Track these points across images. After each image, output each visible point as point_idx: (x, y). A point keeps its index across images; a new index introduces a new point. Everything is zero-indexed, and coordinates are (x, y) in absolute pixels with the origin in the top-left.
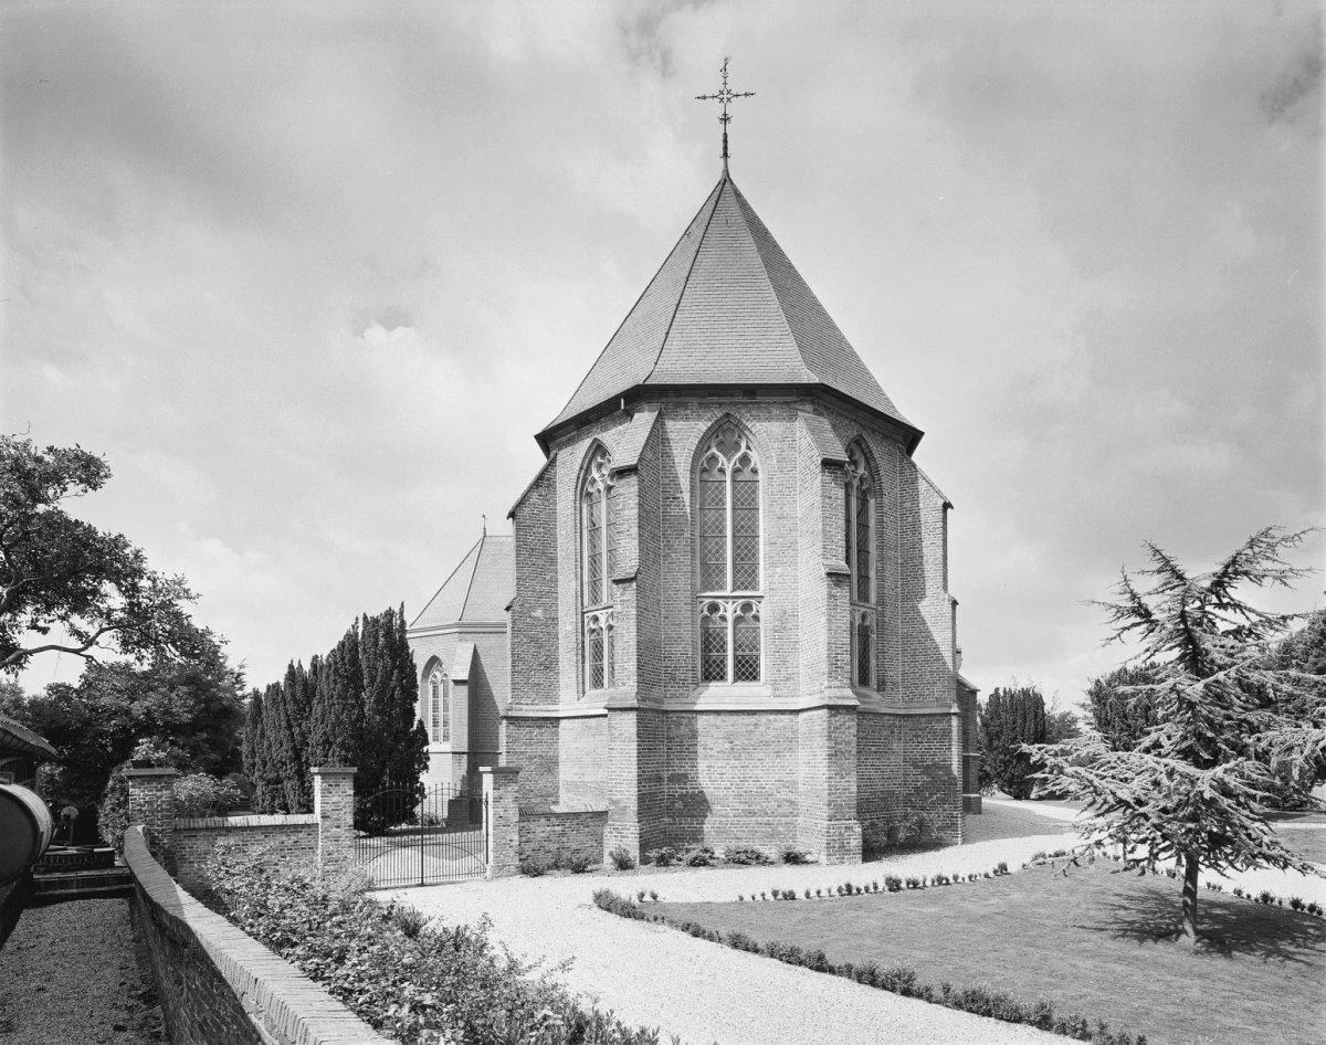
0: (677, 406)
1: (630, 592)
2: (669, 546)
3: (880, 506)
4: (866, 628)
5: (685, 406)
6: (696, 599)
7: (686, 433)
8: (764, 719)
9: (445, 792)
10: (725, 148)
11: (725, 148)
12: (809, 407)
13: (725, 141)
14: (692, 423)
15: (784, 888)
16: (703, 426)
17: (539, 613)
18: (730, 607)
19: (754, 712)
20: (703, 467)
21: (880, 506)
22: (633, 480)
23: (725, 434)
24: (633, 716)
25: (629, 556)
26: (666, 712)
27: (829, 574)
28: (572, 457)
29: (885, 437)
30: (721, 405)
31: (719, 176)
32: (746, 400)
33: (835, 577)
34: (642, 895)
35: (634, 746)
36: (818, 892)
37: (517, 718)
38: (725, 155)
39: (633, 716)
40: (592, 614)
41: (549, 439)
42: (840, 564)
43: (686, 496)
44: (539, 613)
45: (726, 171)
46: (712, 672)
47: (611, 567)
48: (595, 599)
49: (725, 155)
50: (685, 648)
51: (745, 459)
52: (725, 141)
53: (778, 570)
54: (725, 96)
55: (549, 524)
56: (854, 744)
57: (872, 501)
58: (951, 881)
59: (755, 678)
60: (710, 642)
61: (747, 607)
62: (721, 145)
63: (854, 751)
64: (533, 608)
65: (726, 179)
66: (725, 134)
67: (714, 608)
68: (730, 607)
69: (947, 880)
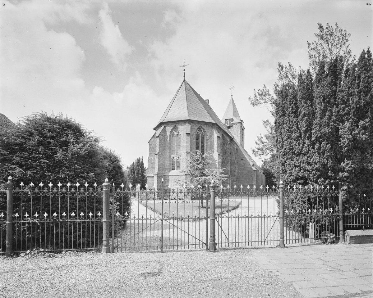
0: (168, 125)
2: (166, 148)
3: (206, 138)
5: (169, 125)
6: (170, 156)
7: (169, 129)
8: (180, 176)
9: (275, 242)
11: (184, 75)
12: (188, 123)
13: (184, 74)
14: (170, 127)
16: (171, 127)
17: (153, 159)
18: (176, 158)
19: (178, 175)
20: (172, 135)
21: (206, 138)
22: (158, 138)
23: (175, 128)
24: (157, 176)
25: (157, 150)
26: (165, 175)
27: (186, 152)
29: (207, 125)
30: (174, 124)
32: (178, 123)
33: (187, 153)
35: (157, 181)
37: (149, 177)
38: (184, 76)
39: (157, 176)
41: (155, 129)
42: (189, 150)
43: (169, 140)
44: (153, 159)
45: (185, 79)
46: (173, 168)
49: (184, 76)
50: (168, 164)
51: (179, 132)
52: (184, 74)
53: (183, 151)
54: (184, 66)
55: (155, 144)
57: (205, 137)
60: (173, 163)
61: (179, 158)
64: (152, 158)
65: (185, 80)
67: (174, 158)
68: (176, 158)
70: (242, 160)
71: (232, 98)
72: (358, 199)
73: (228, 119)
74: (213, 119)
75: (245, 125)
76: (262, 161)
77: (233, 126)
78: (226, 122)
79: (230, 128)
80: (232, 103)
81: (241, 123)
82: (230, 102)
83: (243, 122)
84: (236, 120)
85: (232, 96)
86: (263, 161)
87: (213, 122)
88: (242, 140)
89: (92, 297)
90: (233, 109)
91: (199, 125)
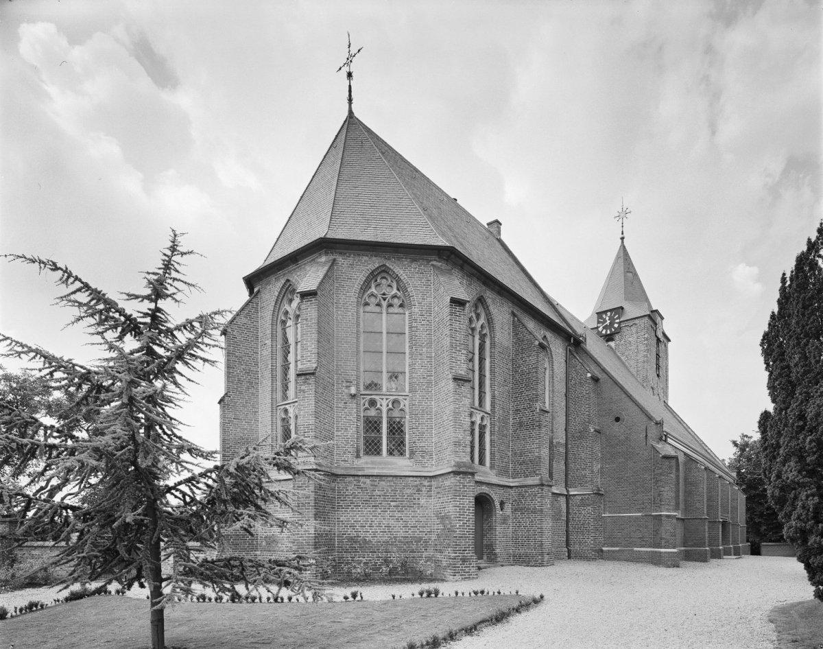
1: (310, 388)
4: (485, 426)
10: (350, 95)
11: (350, 95)
13: (350, 91)
15: (479, 589)
18: (384, 403)
28: (272, 290)
31: (346, 114)
34: (470, 594)
36: (463, 594)
38: (350, 100)
40: (284, 407)
41: (251, 282)
45: (351, 112)
47: (473, 388)
48: (285, 397)
49: (350, 100)
52: (350, 91)
56: (312, 498)
58: (286, 600)
59: (402, 454)
62: (348, 94)
63: (312, 503)
66: (350, 86)
69: (282, 599)
70: (617, 419)
71: (624, 247)
72: (72, 381)
73: (605, 312)
74: (443, 235)
75: (667, 327)
76: (735, 443)
77: (624, 329)
78: (599, 322)
79: (612, 340)
80: (621, 261)
81: (654, 317)
82: (618, 257)
83: (662, 318)
84: (632, 311)
85: (622, 239)
86: (739, 441)
87: (441, 242)
88: (658, 376)
89: (642, 646)
90: (626, 279)
91: (374, 263)
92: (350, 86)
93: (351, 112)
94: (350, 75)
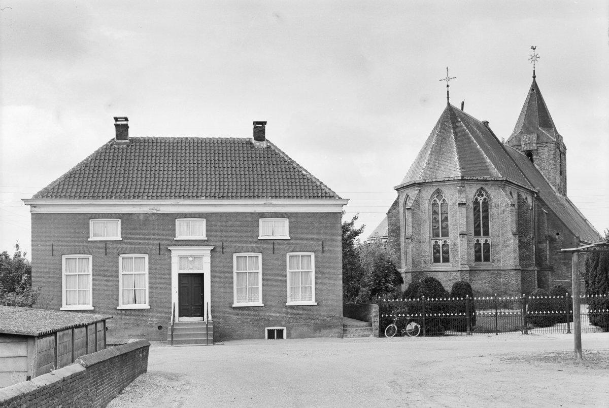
10: (448, 96)
11: (448, 96)
18: (482, 241)
38: (448, 98)
66: (448, 92)
92: (448, 92)
93: (449, 104)
94: (448, 86)
